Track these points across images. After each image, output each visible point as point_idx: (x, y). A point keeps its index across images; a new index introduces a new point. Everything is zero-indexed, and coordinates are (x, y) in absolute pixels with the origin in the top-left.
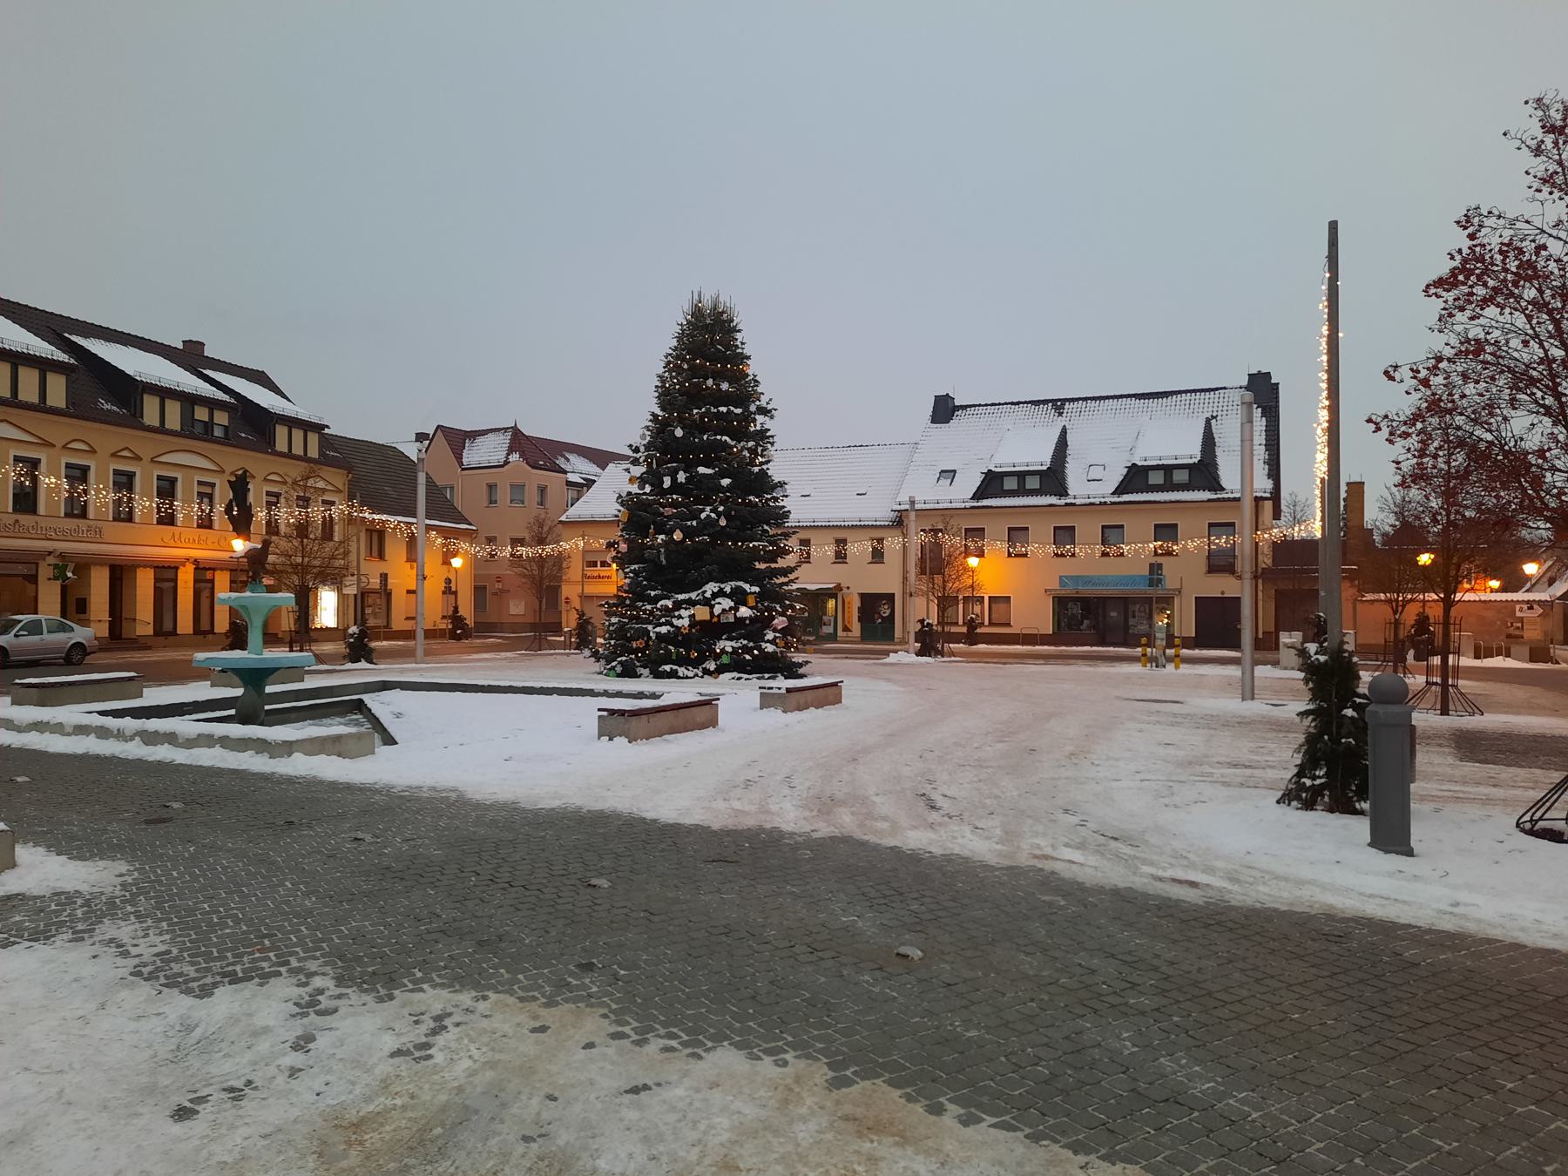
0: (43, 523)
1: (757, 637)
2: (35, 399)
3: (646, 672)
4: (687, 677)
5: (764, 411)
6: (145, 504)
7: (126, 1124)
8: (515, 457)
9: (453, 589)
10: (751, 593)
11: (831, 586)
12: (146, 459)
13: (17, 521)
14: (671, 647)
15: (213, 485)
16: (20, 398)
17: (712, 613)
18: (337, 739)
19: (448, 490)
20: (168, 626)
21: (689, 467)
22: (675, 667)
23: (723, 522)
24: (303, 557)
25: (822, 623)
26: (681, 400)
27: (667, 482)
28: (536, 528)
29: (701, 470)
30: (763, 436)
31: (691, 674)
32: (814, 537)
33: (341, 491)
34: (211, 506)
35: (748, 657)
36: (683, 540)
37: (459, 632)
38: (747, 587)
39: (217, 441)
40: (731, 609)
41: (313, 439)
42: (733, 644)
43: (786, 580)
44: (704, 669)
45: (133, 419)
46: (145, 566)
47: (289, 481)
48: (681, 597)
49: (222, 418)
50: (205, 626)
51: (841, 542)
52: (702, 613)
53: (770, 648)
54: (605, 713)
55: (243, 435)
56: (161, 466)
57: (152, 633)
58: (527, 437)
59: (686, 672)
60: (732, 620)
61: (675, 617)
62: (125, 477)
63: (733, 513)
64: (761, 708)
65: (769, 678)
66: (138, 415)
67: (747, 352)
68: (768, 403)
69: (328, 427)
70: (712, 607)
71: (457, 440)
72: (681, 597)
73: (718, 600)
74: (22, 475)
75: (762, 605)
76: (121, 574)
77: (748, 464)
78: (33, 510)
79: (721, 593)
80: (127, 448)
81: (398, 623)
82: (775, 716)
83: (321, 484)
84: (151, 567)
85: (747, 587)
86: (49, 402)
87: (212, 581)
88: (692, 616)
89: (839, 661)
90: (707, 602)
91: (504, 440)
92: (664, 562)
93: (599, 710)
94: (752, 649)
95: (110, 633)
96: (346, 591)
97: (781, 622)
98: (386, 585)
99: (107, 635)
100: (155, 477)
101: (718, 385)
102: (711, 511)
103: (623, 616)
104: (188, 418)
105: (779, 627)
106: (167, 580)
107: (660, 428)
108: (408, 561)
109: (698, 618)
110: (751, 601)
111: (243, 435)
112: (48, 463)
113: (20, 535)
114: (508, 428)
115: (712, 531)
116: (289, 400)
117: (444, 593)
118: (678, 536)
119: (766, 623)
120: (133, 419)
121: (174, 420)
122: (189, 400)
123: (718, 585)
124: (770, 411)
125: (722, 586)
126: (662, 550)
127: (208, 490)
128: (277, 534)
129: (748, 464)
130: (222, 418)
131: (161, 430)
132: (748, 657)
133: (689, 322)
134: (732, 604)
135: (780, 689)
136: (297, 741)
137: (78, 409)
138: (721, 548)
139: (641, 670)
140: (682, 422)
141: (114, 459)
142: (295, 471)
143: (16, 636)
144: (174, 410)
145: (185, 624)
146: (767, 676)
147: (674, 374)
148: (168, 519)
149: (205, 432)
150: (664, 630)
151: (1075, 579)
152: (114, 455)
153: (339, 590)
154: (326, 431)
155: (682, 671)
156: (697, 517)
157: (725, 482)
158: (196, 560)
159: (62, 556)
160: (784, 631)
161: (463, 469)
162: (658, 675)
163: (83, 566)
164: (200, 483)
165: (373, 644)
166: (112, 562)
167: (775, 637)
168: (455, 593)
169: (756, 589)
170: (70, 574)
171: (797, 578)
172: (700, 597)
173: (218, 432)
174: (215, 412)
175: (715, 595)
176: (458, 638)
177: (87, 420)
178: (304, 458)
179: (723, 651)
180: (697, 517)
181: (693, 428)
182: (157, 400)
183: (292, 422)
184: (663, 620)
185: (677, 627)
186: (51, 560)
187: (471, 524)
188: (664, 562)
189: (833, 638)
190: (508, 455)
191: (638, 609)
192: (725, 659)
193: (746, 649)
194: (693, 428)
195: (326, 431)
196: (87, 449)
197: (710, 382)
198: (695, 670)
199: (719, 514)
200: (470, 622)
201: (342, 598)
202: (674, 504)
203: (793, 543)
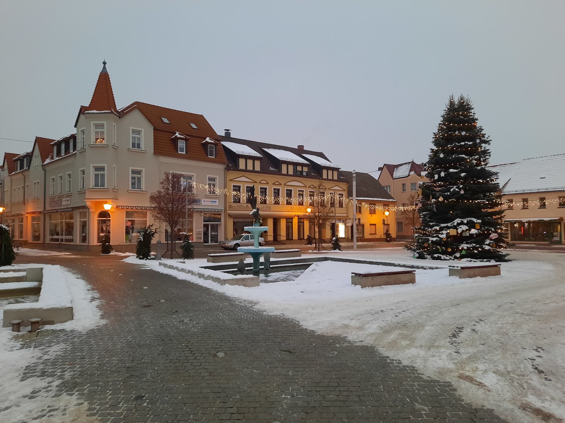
1: (482, 243)
2: (252, 169)
3: (429, 257)
4: (446, 260)
5: (486, 142)
6: (282, 199)
8: (412, 173)
10: (477, 223)
11: (557, 218)
12: (283, 184)
13: (247, 206)
14: (438, 247)
15: (303, 191)
16: (248, 169)
17: (457, 232)
18: (244, 279)
19: (388, 187)
20: (290, 238)
21: (446, 170)
22: (440, 255)
23: (462, 192)
24: (319, 213)
25: (553, 236)
26: (443, 142)
27: (436, 177)
28: (411, 199)
29: (451, 170)
30: (486, 152)
31: (448, 258)
32: (529, 197)
33: (345, 190)
34: (303, 198)
35: (476, 251)
36: (444, 201)
37: (388, 239)
38: (475, 220)
39: (304, 177)
40: (467, 230)
41: (335, 173)
42: (468, 246)
43: (499, 216)
44: (455, 256)
46: (283, 218)
48: (443, 225)
49: (305, 169)
50: (302, 237)
51: (542, 199)
52: (453, 232)
53: (487, 248)
54: (354, 275)
55: (312, 174)
57: (285, 239)
58: (417, 165)
59: (446, 258)
60: (469, 235)
61: (440, 234)
62: (264, 190)
63: (468, 188)
64: (450, 276)
65: (486, 261)
66: (280, 171)
67: (476, 117)
68: (487, 138)
69: (340, 169)
70: (457, 229)
71: (391, 168)
72: (443, 225)
73: (460, 226)
74: (227, 192)
75: (484, 228)
76: (276, 221)
77: (475, 166)
79: (462, 223)
80: (277, 181)
81: (367, 236)
82: (456, 280)
84: (285, 218)
85: (475, 220)
86: (256, 169)
87: (303, 222)
88: (448, 234)
89: (548, 253)
90: (455, 227)
91: (408, 167)
92: (435, 211)
93: (352, 273)
94: (478, 248)
96: (347, 225)
97: (494, 236)
99: (273, 240)
100: (309, 192)
101: (460, 133)
102: (457, 188)
103: (421, 233)
104: (295, 170)
105: (493, 238)
106: (302, 222)
107: (435, 153)
108: (370, 213)
109: (451, 234)
110: (478, 226)
111: (312, 174)
112: (305, 192)
113: (238, 209)
114: (410, 162)
115: (456, 196)
116: (330, 162)
118: (441, 199)
119: (487, 236)
120: (279, 172)
121: (291, 172)
122: (295, 164)
123: (461, 219)
124: (488, 141)
125: (463, 220)
126: (434, 205)
127: (301, 193)
129: (475, 166)
130: (305, 169)
131: (287, 175)
132: (476, 251)
133: (448, 109)
134: (467, 228)
135: (458, 267)
136: (227, 280)
137: (264, 171)
138: (461, 203)
139: (426, 256)
140: (443, 151)
141: (274, 185)
143: (242, 240)
144: (291, 168)
146: (485, 260)
147: (440, 131)
148: (289, 203)
149: (301, 175)
150: (435, 239)
152: (274, 184)
153: (345, 224)
154: (340, 170)
155: (443, 257)
156: (449, 191)
157: (463, 175)
158: (298, 216)
160: (495, 240)
161: (393, 179)
162: (434, 258)
164: (299, 191)
165: (340, 244)
166: (273, 217)
167: (490, 243)
169: (480, 221)
170: (261, 221)
171: (505, 216)
172: (452, 225)
173: (305, 174)
174: (303, 167)
175: (459, 224)
176: (388, 241)
177: (269, 174)
178: (333, 180)
179: (463, 249)
180: (449, 191)
181: (448, 153)
182: (286, 165)
183: (328, 168)
184: (435, 235)
185: (441, 238)
187: (394, 199)
188: (435, 211)
189: (560, 242)
190: (410, 172)
191: (426, 230)
192: (464, 252)
193: (474, 248)
194: (448, 153)
195: (340, 170)
196: (343, 190)
197: (457, 133)
198: (451, 257)
199: (460, 189)
200: (394, 235)
201: (346, 227)
202: (440, 186)
203: (504, 200)
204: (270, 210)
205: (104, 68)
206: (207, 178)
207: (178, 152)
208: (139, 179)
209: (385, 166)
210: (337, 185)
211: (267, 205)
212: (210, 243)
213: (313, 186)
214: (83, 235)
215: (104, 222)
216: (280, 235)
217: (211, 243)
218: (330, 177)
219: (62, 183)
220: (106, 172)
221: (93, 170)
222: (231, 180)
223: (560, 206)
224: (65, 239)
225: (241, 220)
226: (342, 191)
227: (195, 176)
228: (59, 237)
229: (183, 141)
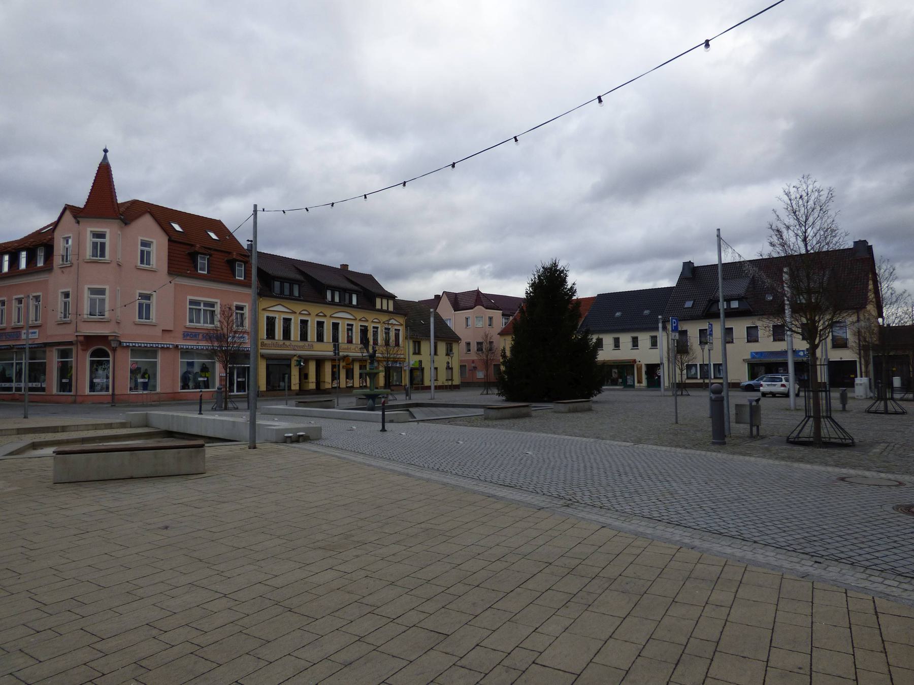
0: (293, 344)
7: (797, 235)
9: (450, 367)
41: (391, 303)
45: (322, 300)
47: (382, 322)
56: (333, 318)
58: (482, 293)
69: (396, 297)
78: (289, 339)
80: (321, 312)
83: (395, 322)
95: (316, 387)
98: (421, 365)
112: (311, 321)
117: (447, 368)
128: (377, 344)
142: (384, 318)
145: (312, 386)
151: (761, 353)
152: (317, 315)
159: (300, 356)
163: (307, 360)
168: (452, 369)
170: (302, 364)
178: (387, 311)
186: (295, 358)
196: (291, 311)
204: (312, 350)
205: (105, 158)
206: (188, 301)
207: (235, 277)
208: (148, 306)
209: (444, 294)
210: (377, 317)
211: (309, 343)
212: (235, 393)
213: (323, 313)
214: (64, 381)
215: (100, 363)
216: (325, 382)
217: (237, 392)
218: (385, 308)
219: (19, 309)
220: (107, 297)
221: (88, 293)
222: (264, 309)
223: (652, 346)
224: (16, 388)
225: (275, 362)
226: (399, 326)
227: (247, 307)
228: (14, 385)
229: (242, 263)
